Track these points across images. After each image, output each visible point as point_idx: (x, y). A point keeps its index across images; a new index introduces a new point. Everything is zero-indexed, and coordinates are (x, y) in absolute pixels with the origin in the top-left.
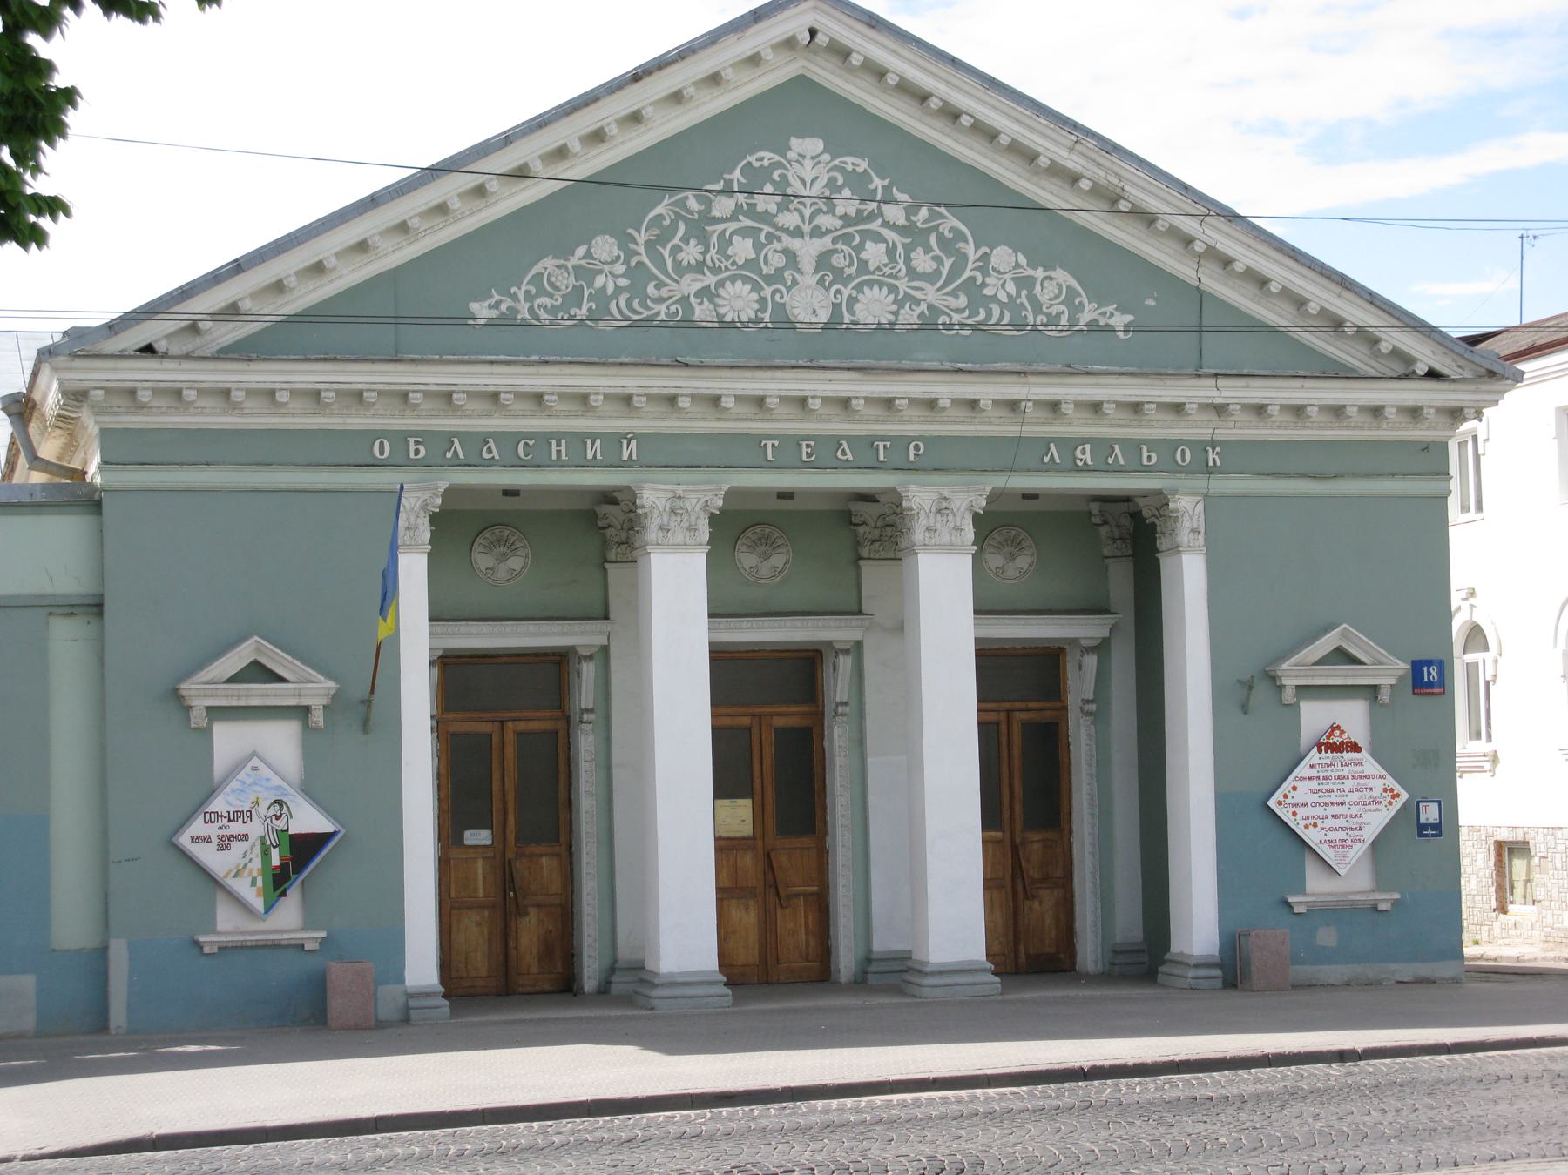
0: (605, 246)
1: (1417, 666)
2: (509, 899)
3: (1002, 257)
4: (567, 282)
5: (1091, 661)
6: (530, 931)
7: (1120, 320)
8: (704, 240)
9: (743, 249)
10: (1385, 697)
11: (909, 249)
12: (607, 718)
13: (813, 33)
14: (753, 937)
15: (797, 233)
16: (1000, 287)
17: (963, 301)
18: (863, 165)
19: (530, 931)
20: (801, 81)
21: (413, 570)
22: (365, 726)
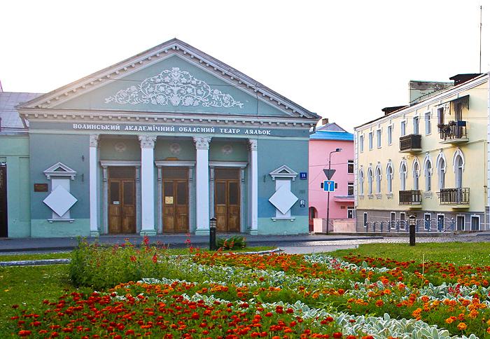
0: (133, 88)
1: (301, 174)
2: (122, 215)
3: (216, 91)
4: (125, 95)
5: (243, 171)
6: (126, 221)
7: (240, 105)
8: (154, 87)
9: (162, 89)
10: (294, 180)
11: (197, 90)
12: (196, 181)
13: (176, 47)
14: (173, 223)
15: (174, 86)
16: (215, 98)
17: (208, 100)
18: (188, 73)
19: (126, 221)
20: (175, 56)
21: (93, 152)
22: (83, 181)
